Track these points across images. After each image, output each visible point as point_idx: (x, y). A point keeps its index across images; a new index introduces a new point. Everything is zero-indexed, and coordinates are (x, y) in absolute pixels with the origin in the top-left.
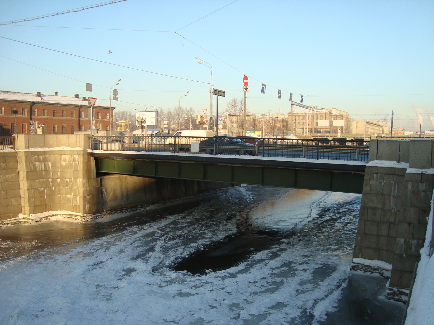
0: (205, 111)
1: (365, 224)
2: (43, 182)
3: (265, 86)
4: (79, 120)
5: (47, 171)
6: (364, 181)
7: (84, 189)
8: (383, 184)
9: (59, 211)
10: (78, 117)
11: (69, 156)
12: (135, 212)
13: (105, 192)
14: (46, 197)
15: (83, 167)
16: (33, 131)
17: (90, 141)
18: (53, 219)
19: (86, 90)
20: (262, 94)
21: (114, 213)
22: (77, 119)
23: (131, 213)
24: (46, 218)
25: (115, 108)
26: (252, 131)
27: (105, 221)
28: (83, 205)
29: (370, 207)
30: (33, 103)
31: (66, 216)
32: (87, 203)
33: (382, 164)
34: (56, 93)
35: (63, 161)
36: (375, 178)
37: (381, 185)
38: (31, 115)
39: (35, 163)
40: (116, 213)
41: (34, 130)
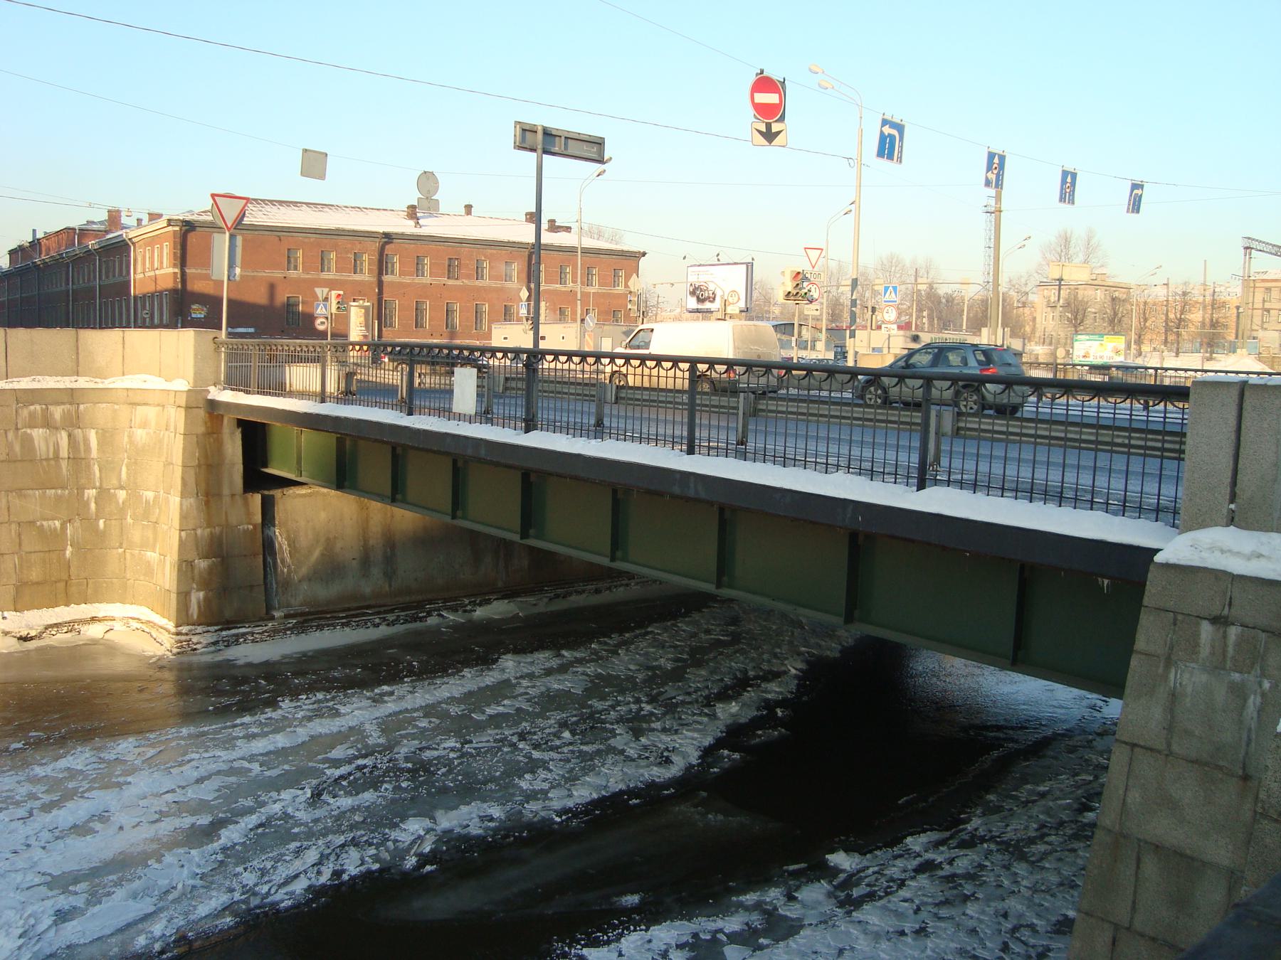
0: (814, 255)
1: (1113, 951)
2: (59, 498)
3: (900, 128)
4: (380, 284)
5: (78, 458)
6: (1134, 662)
7: (183, 534)
8: (1253, 702)
9: (118, 604)
10: (526, 280)
11: (158, 408)
12: (417, 625)
13: (285, 547)
14: (68, 553)
15: (184, 449)
16: (324, 320)
17: (220, 356)
18: (94, 631)
19: (302, 174)
20: (884, 162)
21: (320, 628)
22: (374, 280)
23: (399, 628)
24: (65, 629)
25: (644, 254)
26: (1096, 337)
27: (249, 660)
28: (178, 593)
29: (1157, 848)
30: (388, 237)
31: (139, 626)
32: (195, 586)
33: (1260, 556)
34: (469, 209)
35: (140, 428)
36: (1205, 651)
37: (1243, 706)
38: (380, 273)
39: (29, 431)
40: (328, 625)
41: (327, 318)
